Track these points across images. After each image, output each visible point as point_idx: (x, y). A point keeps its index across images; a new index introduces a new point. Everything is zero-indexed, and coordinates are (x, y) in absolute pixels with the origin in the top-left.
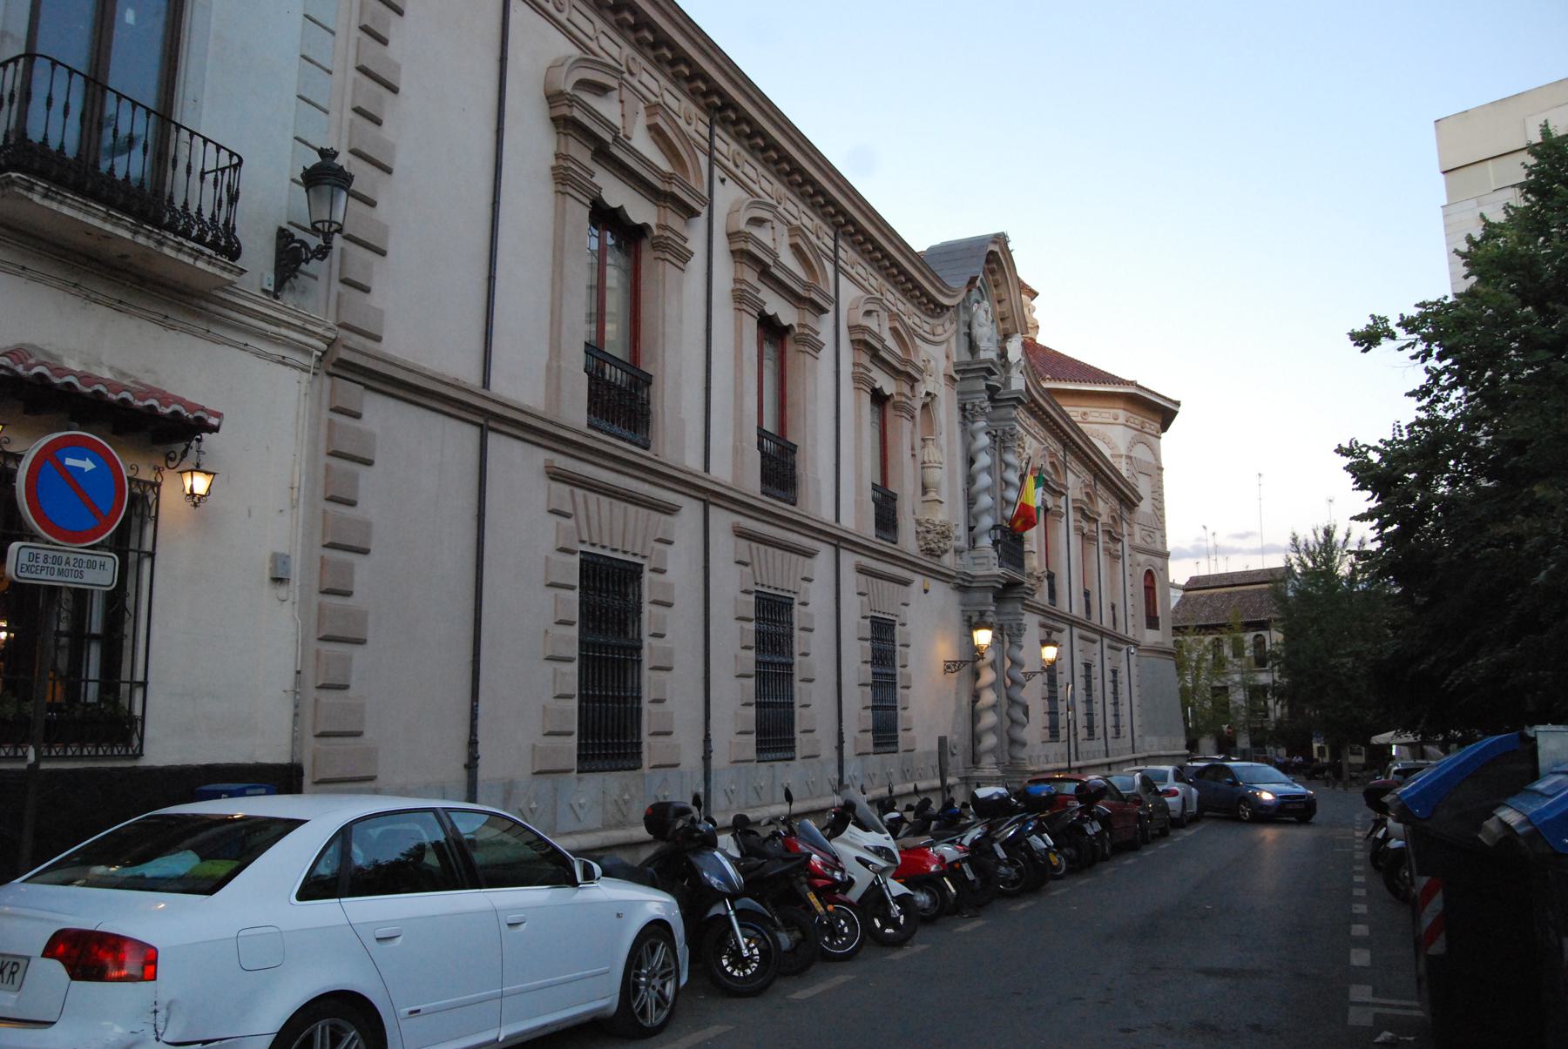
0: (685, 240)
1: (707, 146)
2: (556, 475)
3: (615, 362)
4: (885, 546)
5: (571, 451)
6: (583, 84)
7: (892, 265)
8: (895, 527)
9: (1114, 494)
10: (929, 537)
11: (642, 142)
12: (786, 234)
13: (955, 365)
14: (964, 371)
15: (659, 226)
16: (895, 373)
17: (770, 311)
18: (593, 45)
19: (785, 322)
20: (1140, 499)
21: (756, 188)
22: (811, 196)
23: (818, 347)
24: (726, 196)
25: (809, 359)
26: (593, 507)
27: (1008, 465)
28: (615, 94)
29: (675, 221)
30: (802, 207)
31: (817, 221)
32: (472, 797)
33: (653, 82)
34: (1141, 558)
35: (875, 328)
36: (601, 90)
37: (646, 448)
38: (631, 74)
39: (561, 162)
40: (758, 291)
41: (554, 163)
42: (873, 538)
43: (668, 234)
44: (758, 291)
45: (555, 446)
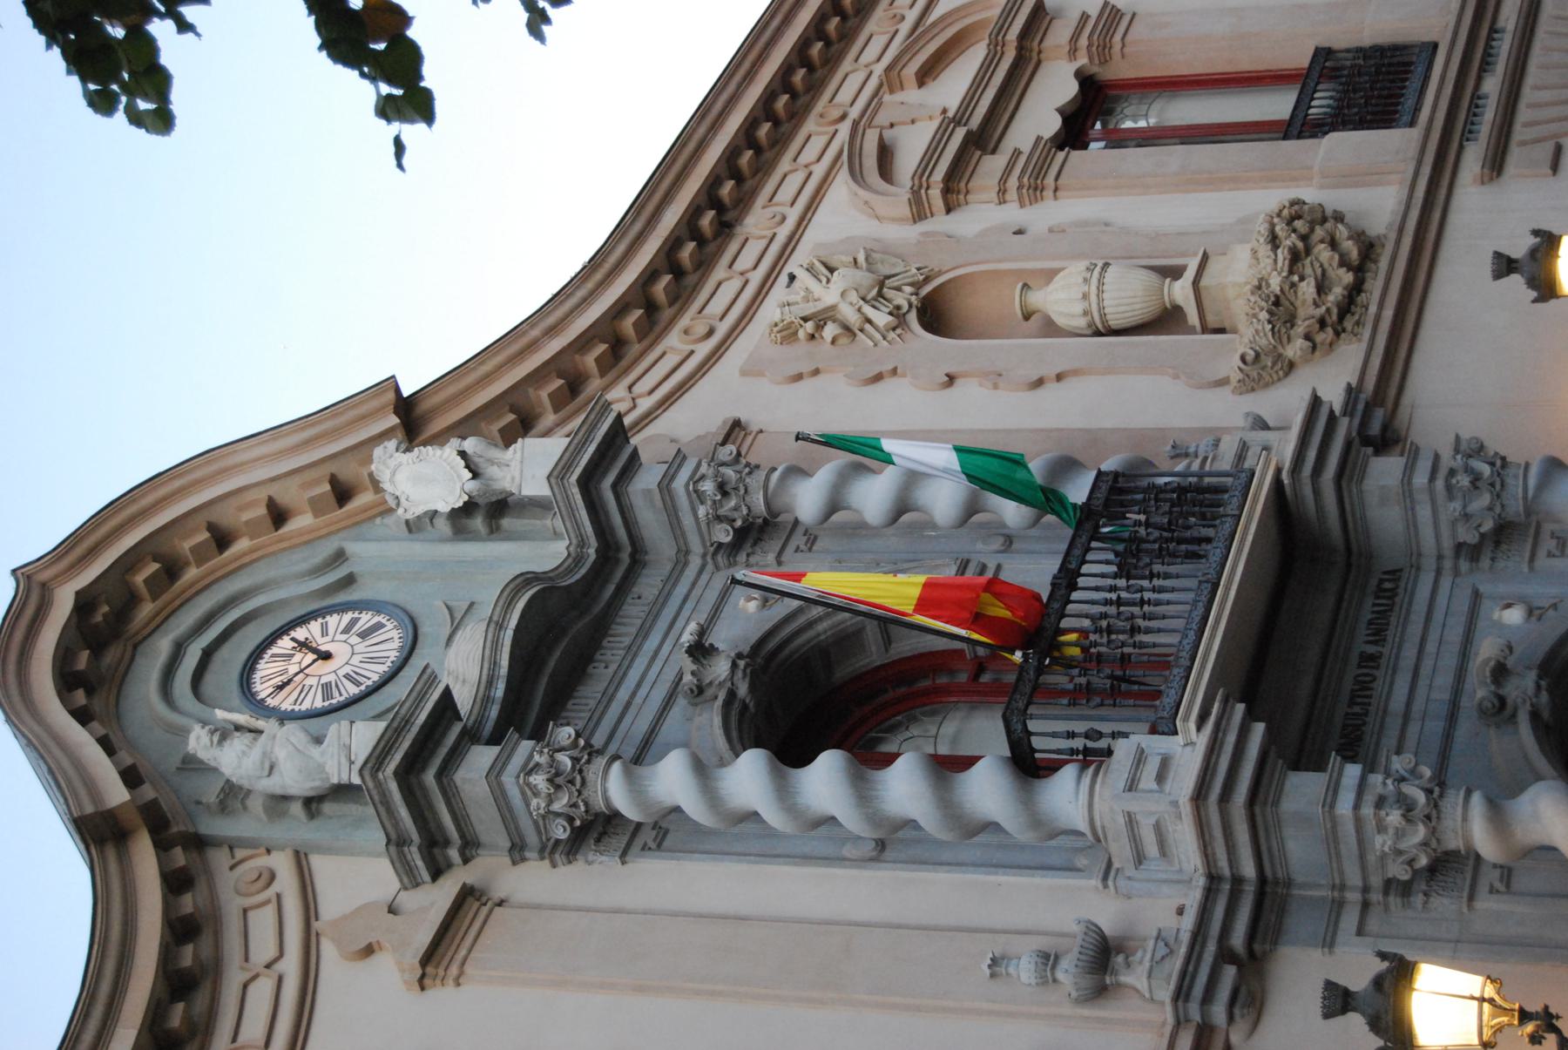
0: (1085, 17)
2: (1496, 164)
3: (1302, 104)
4: (1433, 101)
5: (1432, 235)
11: (952, 87)
12: (899, 96)
13: (410, 881)
14: (433, 843)
16: (1024, 68)
19: (1071, 89)
21: (819, 171)
22: (828, 43)
25: (1138, 31)
26: (1546, 95)
27: (834, 505)
28: (887, 134)
29: (1059, 35)
30: (785, 164)
31: (810, 125)
33: (851, 84)
36: (885, 155)
38: (711, 332)
40: (1017, 153)
42: (1415, 134)
44: (1017, 153)
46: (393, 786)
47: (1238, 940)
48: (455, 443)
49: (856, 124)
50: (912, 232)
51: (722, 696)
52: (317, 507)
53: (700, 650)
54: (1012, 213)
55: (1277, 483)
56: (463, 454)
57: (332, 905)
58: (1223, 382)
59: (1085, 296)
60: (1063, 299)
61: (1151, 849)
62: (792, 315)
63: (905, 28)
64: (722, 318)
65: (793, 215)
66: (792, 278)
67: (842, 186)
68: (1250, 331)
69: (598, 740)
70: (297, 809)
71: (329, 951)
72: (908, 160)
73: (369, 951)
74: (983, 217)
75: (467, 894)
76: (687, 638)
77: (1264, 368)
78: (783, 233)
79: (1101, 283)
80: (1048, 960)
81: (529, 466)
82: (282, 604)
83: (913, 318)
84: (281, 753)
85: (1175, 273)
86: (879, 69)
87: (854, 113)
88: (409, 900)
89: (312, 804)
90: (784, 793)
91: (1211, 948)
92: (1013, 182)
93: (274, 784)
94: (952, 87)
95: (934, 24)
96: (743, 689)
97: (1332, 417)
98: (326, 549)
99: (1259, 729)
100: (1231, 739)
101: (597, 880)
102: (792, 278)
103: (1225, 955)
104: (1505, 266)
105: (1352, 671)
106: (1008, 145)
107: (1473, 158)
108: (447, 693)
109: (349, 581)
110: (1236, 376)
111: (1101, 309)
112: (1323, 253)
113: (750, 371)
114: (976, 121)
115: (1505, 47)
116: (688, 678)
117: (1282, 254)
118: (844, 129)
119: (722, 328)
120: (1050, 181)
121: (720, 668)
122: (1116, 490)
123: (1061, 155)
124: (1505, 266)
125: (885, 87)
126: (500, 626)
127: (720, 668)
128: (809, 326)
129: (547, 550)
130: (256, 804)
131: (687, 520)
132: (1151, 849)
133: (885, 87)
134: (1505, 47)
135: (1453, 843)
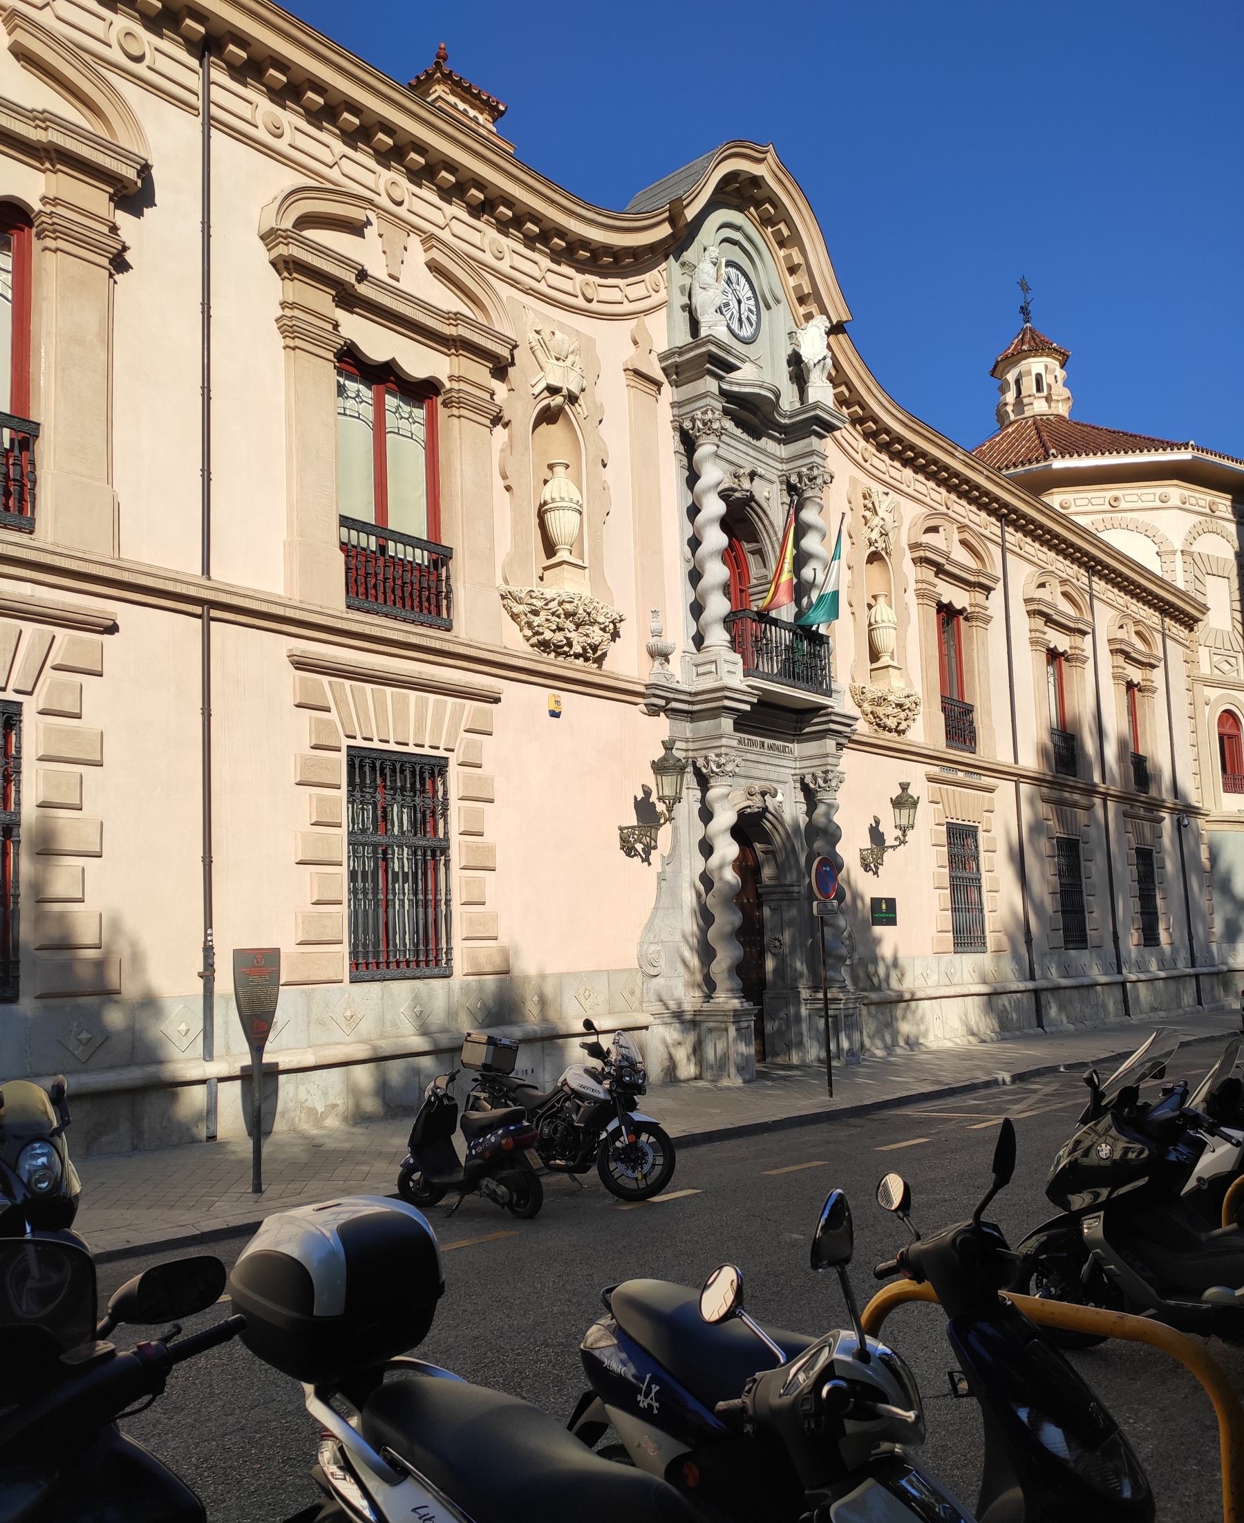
0: (986, 609)
1: (999, 541)
2: (301, 664)
6: (307, 221)
7: (906, 448)
8: (973, 739)
9: (1151, 606)
10: (537, 621)
11: (961, 555)
15: (971, 605)
17: (945, 601)
18: (334, 174)
19: (958, 606)
20: (1204, 609)
21: (927, 500)
23: (1153, 690)
24: (1022, 577)
26: (957, 797)
29: (979, 597)
32: (1193, 966)
33: (963, 510)
34: (1213, 693)
35: (1048, 598)
36: (934, 529)
37: (448, 630)
39: (288, 312)
41: (280, 312)
43: (977, 609)
45: (431, 658)
46: (703, 349)
47: (674, 705)
48: (830, 354)
49: (946, 515)
50: (904, 544)
51: (735, 486)
52: (798, 288)
53: (753, 475)
54: (912, 586)
55: (827, 707)
56: (824, 358)
57: (649, 320)
58: (854, 681)
59: (562, 499)
60: (883, 612)
61: (701, 670)
62: (875, 499)
63: (982, 530)
64: (149, 68)
65: (1104, 597)
66: (887, 494)
67: (921, 510)
68: (874, 689)
69: (723, 438)
70: (686, 300)
71: (632, 324)
72: (930, 539)
73: (635, 343)
74: (911, 572)
75: (658, 385)
76: (760, 471)
77: (859, 696)
78: (903, 487)
79: (569, 509)
80: (657, 634)
81: (821, 391)
82: (758, 276)
83: (873, 549)
84: (711, 292)
85: (892, 658)
86: (967, 521)
87: (950, 512)
88: (654, 357)
89: (689, 309)
90: (710, 521)
91: (671, 696)
92: (925, 586)
93: (697, 291)
94: (961, 555)
95: (488, 283)
96: (737, 495)
97: (849, 726)
98: (781, 296)
99: (748, 708)
100: (745, 698)
101: (669, 442)
102: (887, 494)
103: (668, 700)
104: (904, 787)
105: (759, 739)
106: (340, 315)
107: (934, 770)
108: (739, 368)
109: (768, 307)
110: (856, 685)
111: (558, 509)
112: (903, 715)
113: (854, 481)
114: (363, 289)
115: (974, 780)
116: (742, 471)
117: (902, 700)
118: (945, 510)
119: (867, 465)
120: (926, 601)
121: (746, 484)
122: (819, 640)
123: (331, 356)
124: (904, 787)
125: (424, 236)
126: (761, 387)
127: (746, 484)
128: (870, 505)
129: (789, 401)
130: (687, 281)
131: (799, 463)
132: (701, 670)
133: (424, 236)
134: (974, 780)
135: (712, 782)
